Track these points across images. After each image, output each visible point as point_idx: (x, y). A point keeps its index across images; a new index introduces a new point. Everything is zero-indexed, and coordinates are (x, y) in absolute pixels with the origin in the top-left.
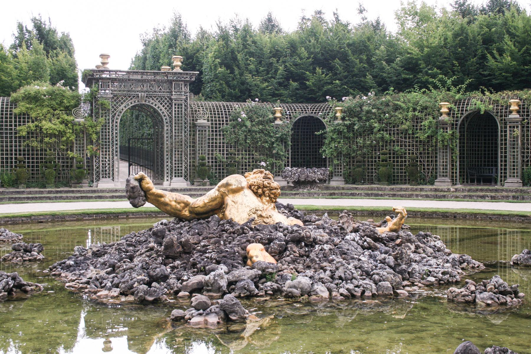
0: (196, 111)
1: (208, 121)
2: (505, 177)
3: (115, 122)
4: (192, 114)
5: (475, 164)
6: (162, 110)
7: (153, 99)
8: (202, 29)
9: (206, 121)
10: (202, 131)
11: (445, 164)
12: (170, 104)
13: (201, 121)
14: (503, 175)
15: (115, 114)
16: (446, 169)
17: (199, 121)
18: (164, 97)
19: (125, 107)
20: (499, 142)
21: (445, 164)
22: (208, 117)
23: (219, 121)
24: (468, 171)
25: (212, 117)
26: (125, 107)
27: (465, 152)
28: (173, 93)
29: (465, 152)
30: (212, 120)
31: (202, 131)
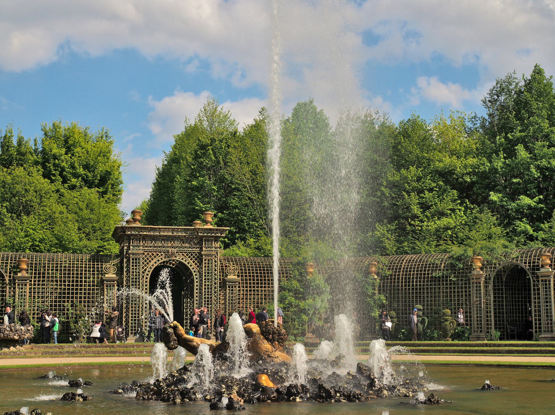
0: (226, 266)
1: (238, 276)
2: (540, 331)
3: (145, 278)
4: (223, 269)
5: (516, 320)
6: (192, 266)
7: (183, 255)
8: (311, 102)
9: (236, 277)
10: (546, 281)
11: (479, 319)
12: (200, 259)
13: (231, 277)
14: (538, 330)
15: (145, 270)
16: (481, 324)
17: (229, 277)
18: (194, 253)
19: (155, 263)
20: (533, 296)
21: (479, 319)
22: (239, 273)
23: (261, 276)
24: (508, 326)
25: (242, 273)
26: (155, 263)
27: (505, 307)
28: (204, 249)
29: (505, 307)
30: (242, 276)
31: (546, 281)
